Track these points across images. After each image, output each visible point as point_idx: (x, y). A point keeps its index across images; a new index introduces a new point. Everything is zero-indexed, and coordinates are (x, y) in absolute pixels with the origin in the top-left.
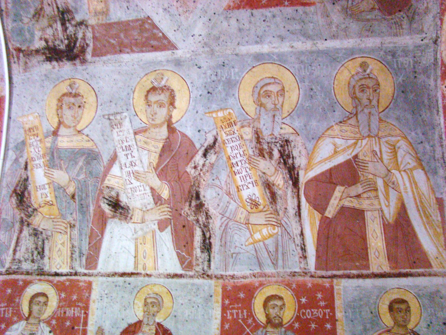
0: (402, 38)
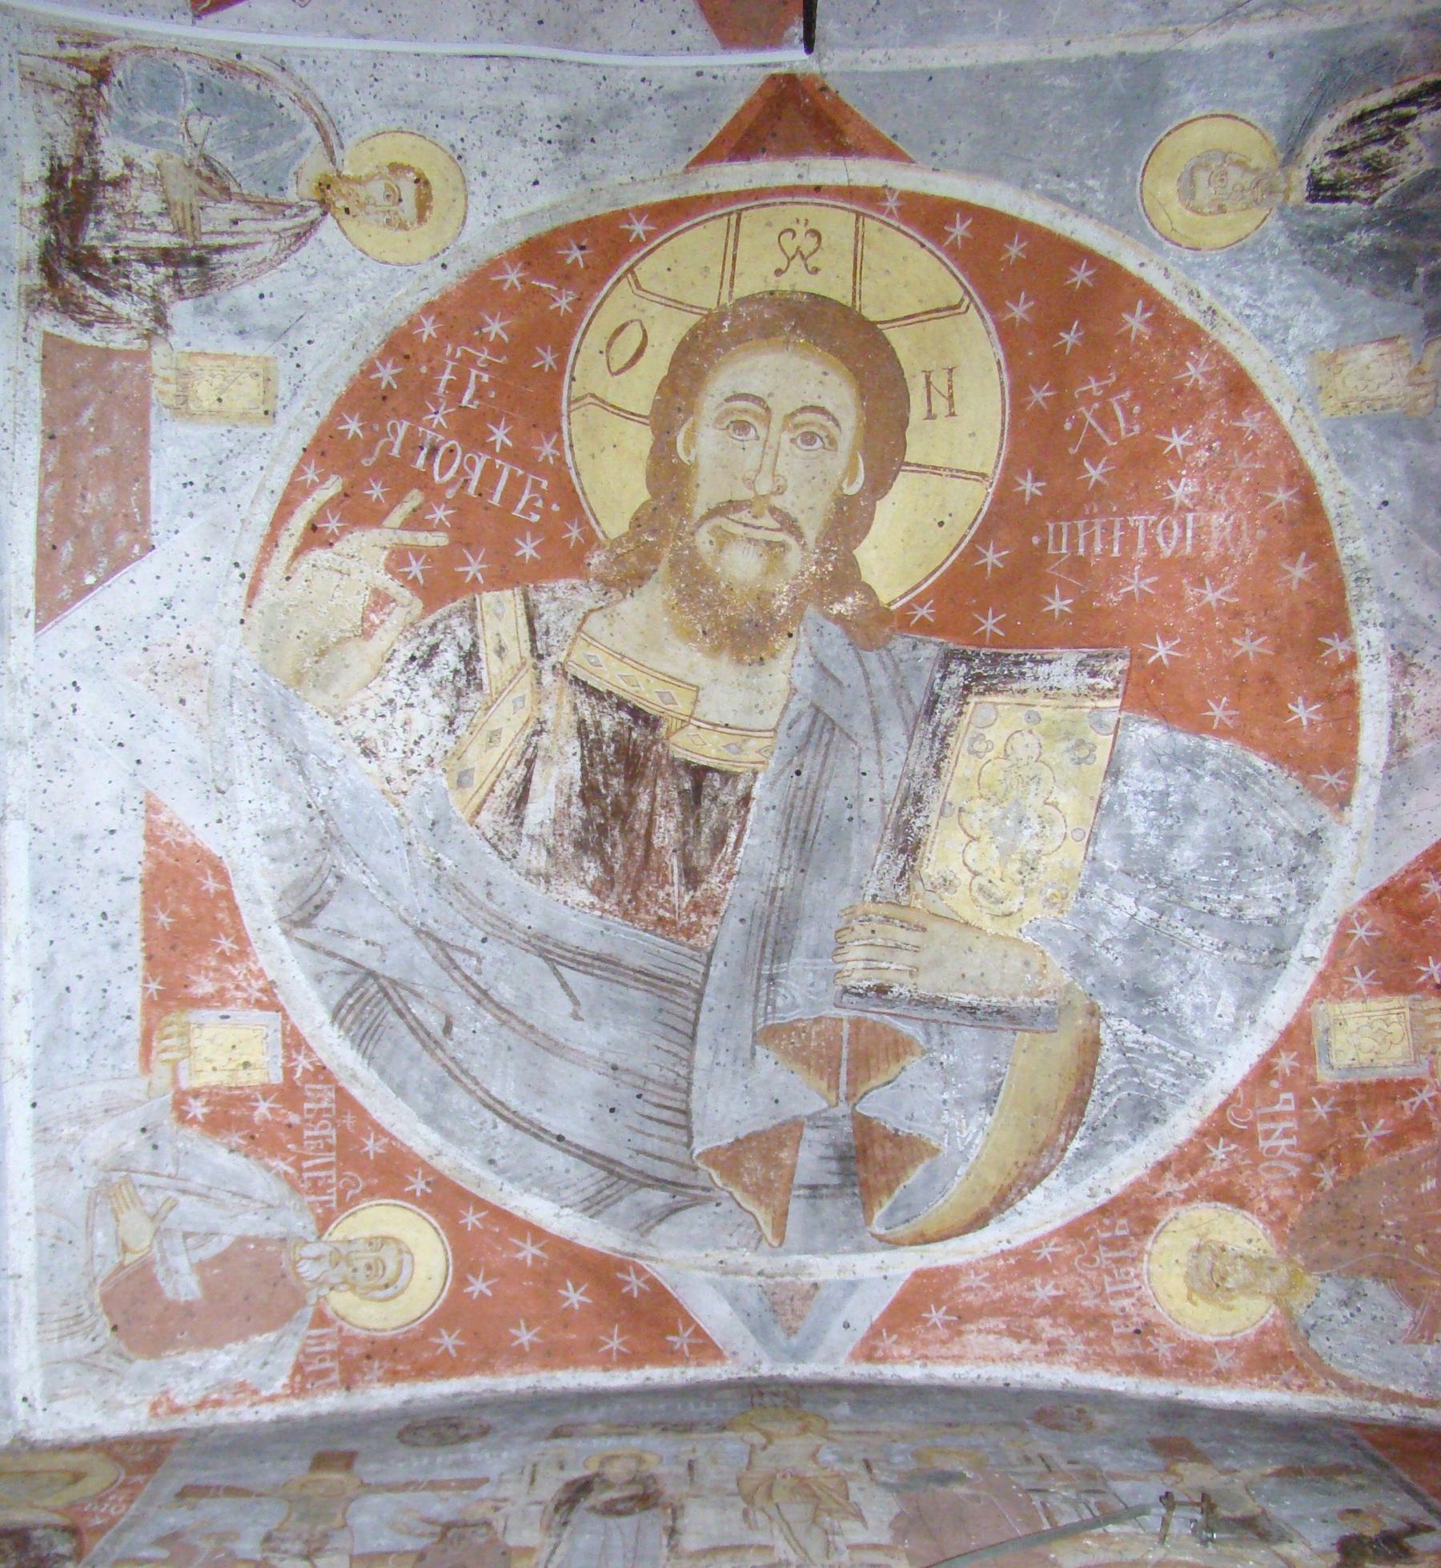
0: (33, 1338)
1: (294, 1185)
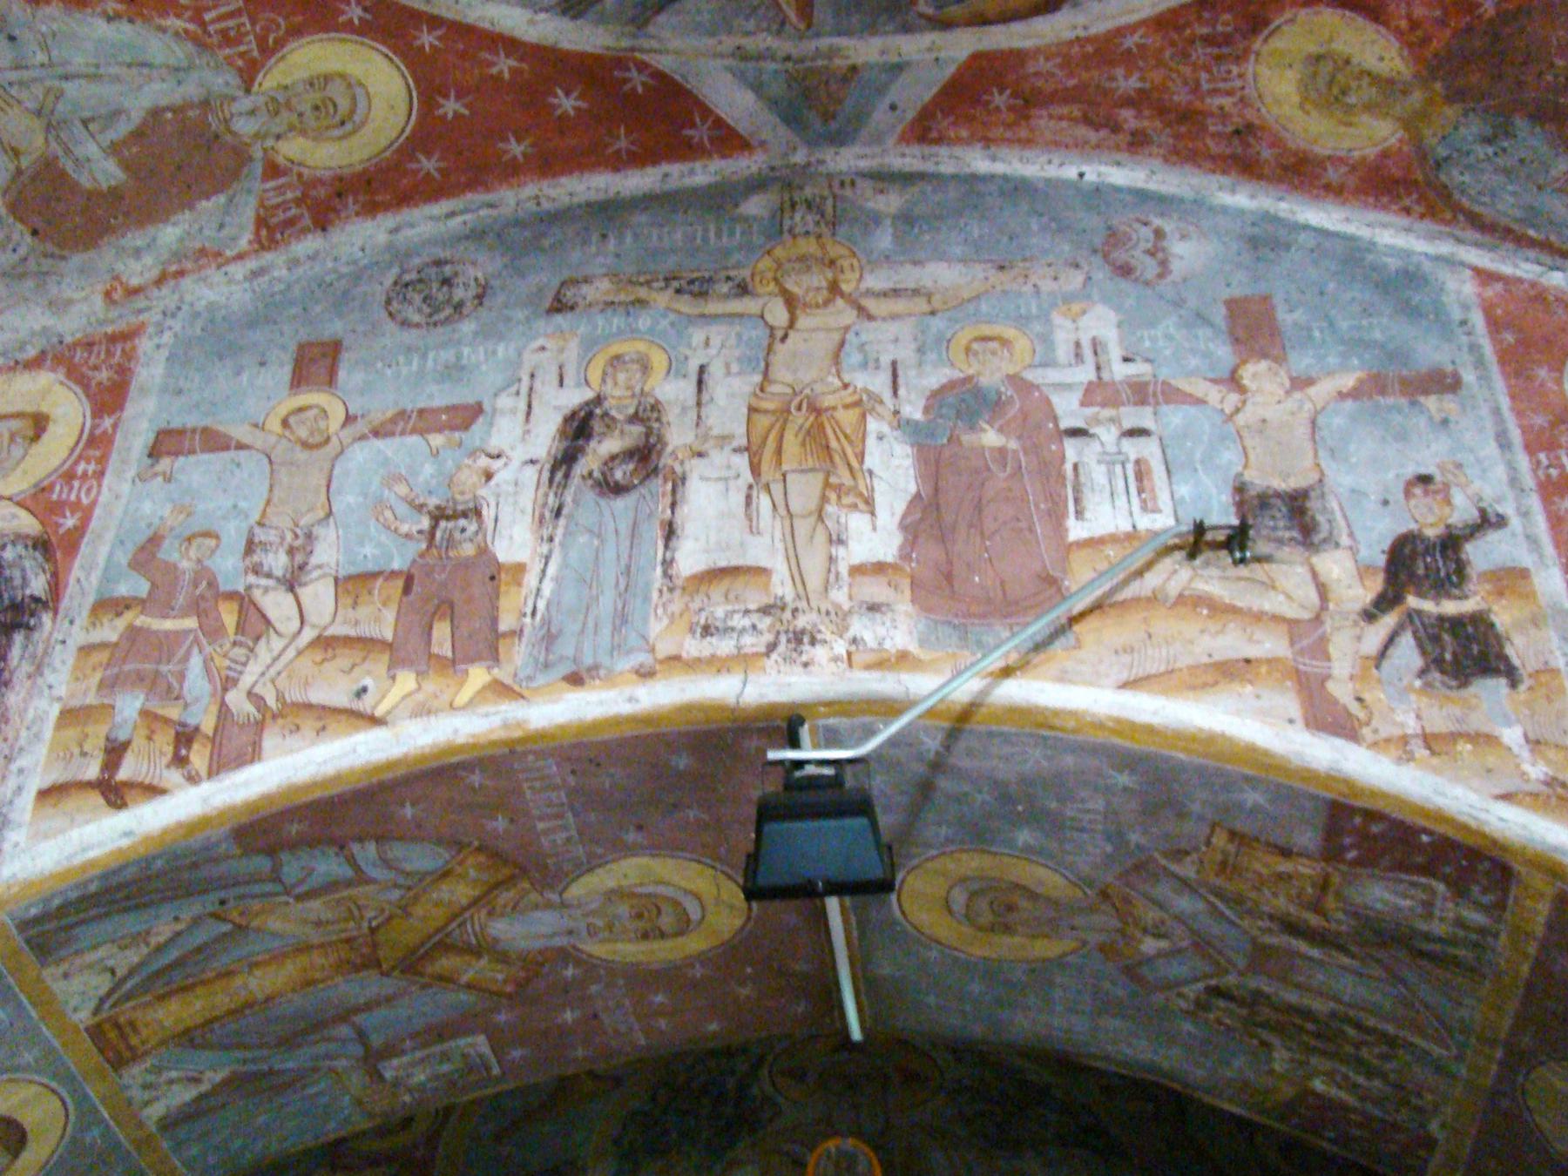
1: (201, 44)
